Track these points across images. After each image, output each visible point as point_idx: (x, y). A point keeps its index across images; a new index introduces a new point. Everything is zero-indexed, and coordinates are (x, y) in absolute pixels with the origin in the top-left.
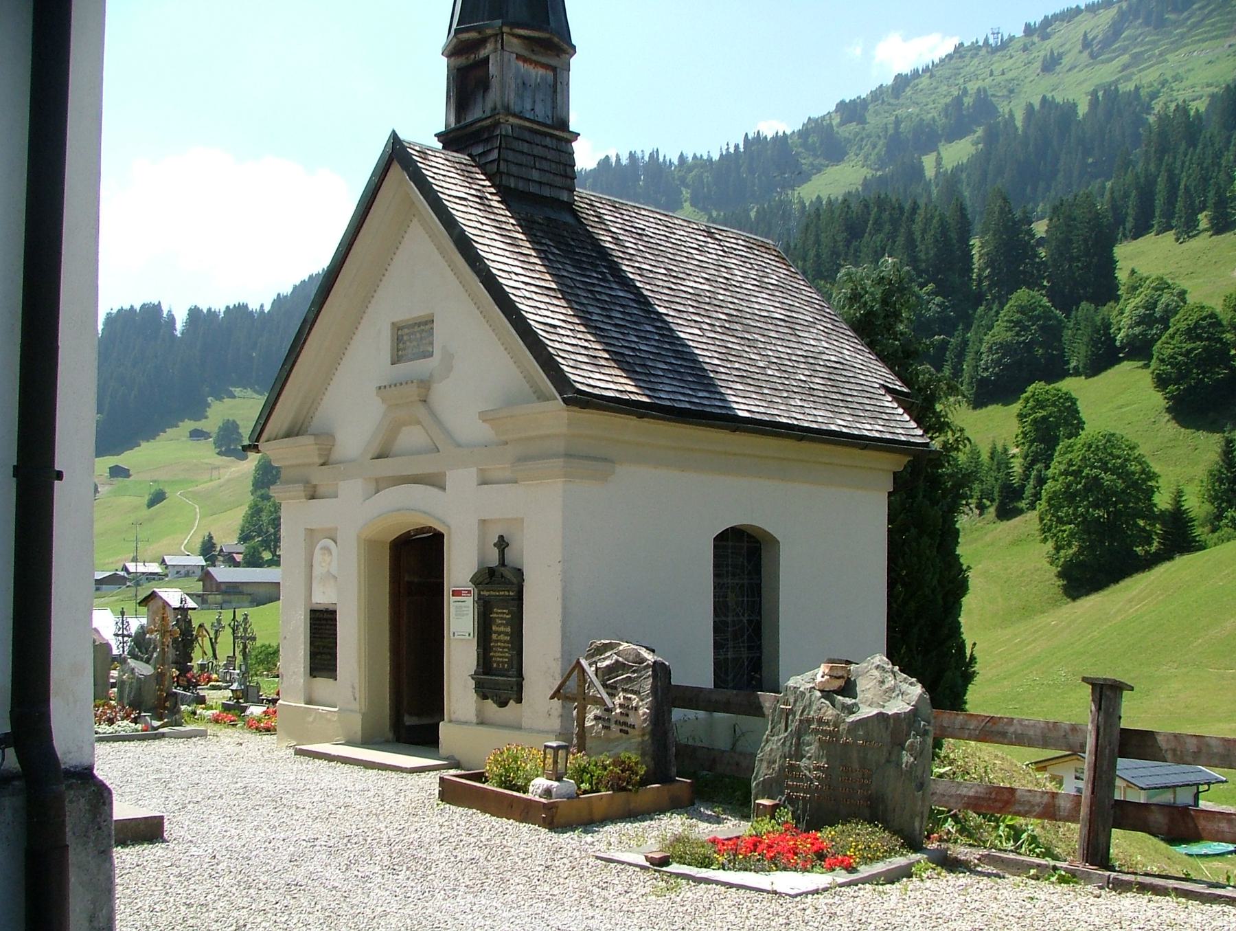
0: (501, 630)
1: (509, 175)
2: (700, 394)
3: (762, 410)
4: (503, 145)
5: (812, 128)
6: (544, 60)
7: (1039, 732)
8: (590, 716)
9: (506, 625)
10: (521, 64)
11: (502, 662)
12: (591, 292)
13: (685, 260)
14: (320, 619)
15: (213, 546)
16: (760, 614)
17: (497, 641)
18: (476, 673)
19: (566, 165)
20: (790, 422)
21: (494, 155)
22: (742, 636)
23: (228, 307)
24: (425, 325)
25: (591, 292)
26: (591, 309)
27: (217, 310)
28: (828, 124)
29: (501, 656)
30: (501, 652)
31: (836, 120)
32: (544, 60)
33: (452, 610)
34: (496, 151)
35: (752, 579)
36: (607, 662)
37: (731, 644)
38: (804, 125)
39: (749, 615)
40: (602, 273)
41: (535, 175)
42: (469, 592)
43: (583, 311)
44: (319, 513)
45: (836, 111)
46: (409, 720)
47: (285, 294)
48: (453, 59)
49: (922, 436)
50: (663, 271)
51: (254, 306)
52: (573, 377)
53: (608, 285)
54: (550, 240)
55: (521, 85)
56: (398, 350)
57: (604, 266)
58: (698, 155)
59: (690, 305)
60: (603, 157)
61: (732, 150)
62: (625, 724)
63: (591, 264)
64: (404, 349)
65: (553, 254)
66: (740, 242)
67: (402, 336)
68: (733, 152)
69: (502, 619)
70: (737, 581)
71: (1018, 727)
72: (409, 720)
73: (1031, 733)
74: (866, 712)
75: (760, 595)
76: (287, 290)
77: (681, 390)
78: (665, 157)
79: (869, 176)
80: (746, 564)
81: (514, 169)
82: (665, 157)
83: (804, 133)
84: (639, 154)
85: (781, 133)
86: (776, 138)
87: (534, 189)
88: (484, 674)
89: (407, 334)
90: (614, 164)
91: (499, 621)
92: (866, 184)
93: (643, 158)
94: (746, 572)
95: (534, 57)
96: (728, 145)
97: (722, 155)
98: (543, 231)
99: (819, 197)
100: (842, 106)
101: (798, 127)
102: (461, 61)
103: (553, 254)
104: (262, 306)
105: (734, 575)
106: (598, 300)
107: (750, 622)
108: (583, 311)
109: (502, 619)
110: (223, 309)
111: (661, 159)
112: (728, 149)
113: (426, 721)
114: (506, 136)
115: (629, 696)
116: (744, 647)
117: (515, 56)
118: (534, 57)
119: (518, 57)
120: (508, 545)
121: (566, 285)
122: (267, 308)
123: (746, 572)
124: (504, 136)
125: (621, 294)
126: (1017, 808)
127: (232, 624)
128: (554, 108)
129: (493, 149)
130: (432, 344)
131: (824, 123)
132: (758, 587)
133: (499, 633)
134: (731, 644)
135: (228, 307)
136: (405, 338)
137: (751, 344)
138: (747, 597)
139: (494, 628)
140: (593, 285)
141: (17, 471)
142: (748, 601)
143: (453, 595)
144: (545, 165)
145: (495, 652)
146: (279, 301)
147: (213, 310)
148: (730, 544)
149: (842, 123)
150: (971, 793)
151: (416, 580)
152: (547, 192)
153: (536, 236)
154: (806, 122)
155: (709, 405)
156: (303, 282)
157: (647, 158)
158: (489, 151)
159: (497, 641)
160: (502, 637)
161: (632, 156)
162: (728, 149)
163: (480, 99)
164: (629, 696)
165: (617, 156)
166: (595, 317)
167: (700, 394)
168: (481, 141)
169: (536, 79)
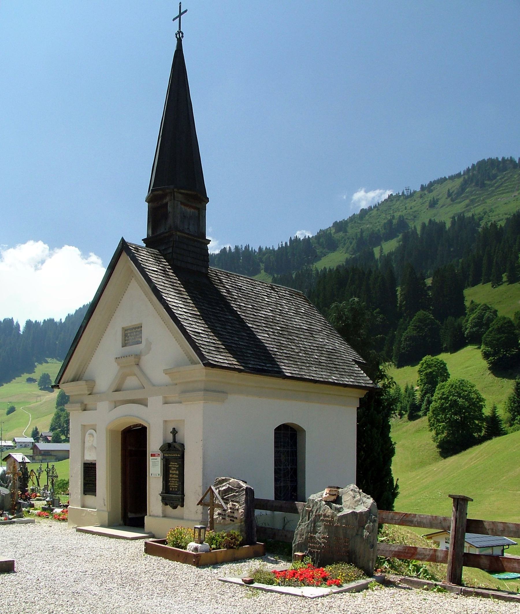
0: (174, 473)
3: (297, 372)
7: (428, 521)
8: (216, 513)
9: (176, 470)
11: (174, 488)
12: (216, 316)
13: (261, 301)
14: (88, 467)
16: (296, 465)
17: (172, 478)
23: (45, 320)
24: (138, 328)
25: (216, 316)
27: (40, 322)
30: (174, 483)
31: (333, 231)
33: (151, 463)
39: (291, 466)
40: (222, 308)
42: (159, 454)
45: (333, 226)
47: (72, 314)
50: (251, 307)
51: (57, 320)
56: (125, 341)
58: (268, 247)
62: (233, 517)
64: (128, 340)
66: (287, 292)
67: (127, 334)
69: (174, 467)
71: (419, 518)
74: (347, 511)
75: (296, 456)
78: (252, 248)
82: (252, 248)
83: (318, 237)
84: (240, 247)
89: (129, 333)
92: (347, 261)
100: (336, 224)
106: (219, 320)
107: (291, 469)
109: (174, 467)
110: (42, 321)
116: (289, 481)
122: (63, 321)
130: (141, 337)
131: (327, 232)
133: (173, 474)
134: (282, 479)
135: (45, 320)
136: (129, 335)
137: (292, 341)
138: (291, 457)
139: (171, 472)
142: (290, 459)
143: (151, 456)
145: (171, 483)
146: (69, 317)
147: (38, 321)
149: (335, 233)
150: (396, 550)
151: (134, 449)
156: (80, 308)
159: (172, 478)
160: (174, 476)
161: (237, 247)
164: (235, 503)
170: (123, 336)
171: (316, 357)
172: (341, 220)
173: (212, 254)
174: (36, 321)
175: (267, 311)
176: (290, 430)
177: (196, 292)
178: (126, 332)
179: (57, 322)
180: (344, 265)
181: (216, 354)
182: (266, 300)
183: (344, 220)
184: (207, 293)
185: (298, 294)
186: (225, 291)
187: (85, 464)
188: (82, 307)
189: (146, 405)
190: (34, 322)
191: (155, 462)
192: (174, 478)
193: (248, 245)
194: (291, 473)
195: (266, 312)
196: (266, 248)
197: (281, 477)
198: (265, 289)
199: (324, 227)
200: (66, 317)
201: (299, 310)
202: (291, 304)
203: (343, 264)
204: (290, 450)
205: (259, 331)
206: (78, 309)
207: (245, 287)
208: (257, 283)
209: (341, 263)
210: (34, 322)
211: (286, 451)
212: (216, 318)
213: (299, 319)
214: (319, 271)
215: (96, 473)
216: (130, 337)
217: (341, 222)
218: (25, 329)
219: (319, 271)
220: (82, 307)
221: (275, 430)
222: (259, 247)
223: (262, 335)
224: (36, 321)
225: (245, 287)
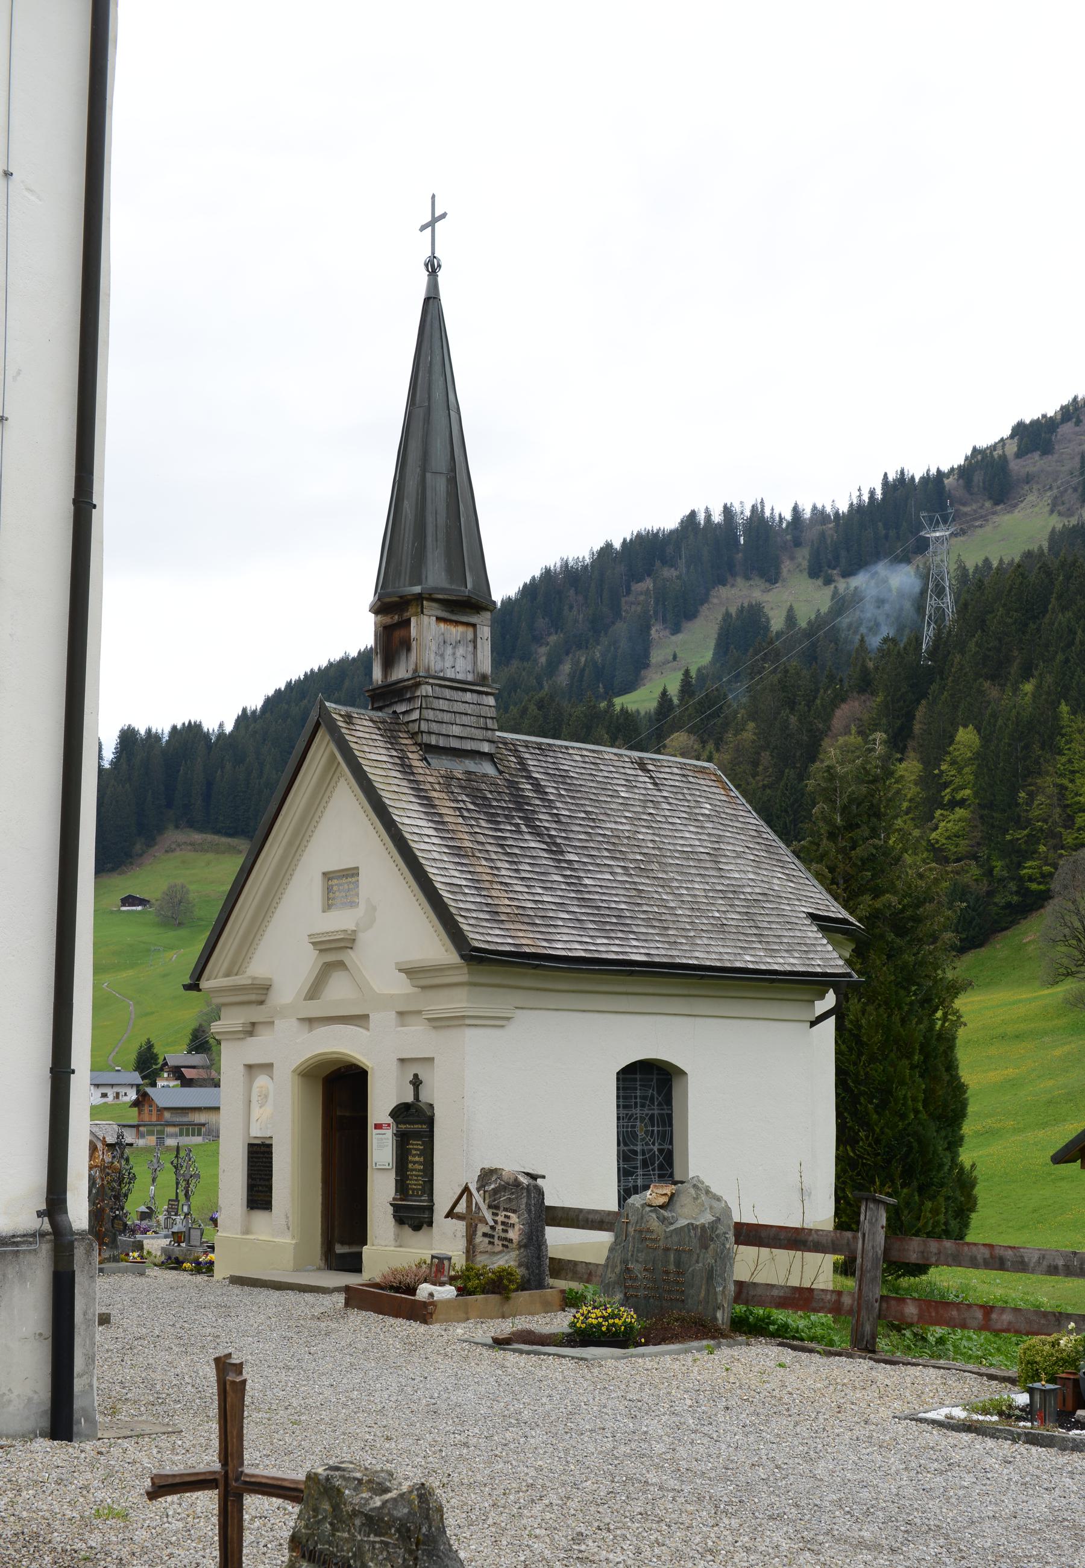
0: (415, 1159)
1: (430, 733)
2: (599, 941)
3: (663, 952)
4: (424, 706)
5: (977, 462)
6: (464, 619)
7: (829, 1239)
8: (479, 1233)
9: (419, 1156)
10: (442, 625)
11: (417, 1189)
12: (502, 846)
13: (609, 799)
14: (257, 1153)
15: (154, 1057)
16: (671, 1143)
17: (412, 1170)
18: (394, 1199)
19: (486, 717)
20: (691, 962)
21: (415, 715)
22: (653, 1164)
23: (174, 728)
24: (352, 873)
25: (502, 846)
26: (499, 864)
27: (160, 731)
28: (1000, 456)
29: (415, 1183)
30: (416, 1180)
31: (1012, 448)
32: (464, 619)
33: (375, 1141)
34: (418, 711)
35: (662, 1109)
36: (492, 1186)
37: (640, 1172)
38: (967, 458)
39: (660, 1144)
40: (517, 825)
41: (456, 730)
42: (389, 1125)
43: (491, 868)
44: (255, 1050)
45: (1012, 436)
46: (340, 1249)
47: (253, 708)
48: (379, 616)
49: (843, 966)
50: (583, 815)
51: (210, 725)
52: (471, 935)
53: (521, 837)
54: (467, 795)
55: (442, 644)
56: (329, 899)
57: (519, 817)
58: (819, 506)
59: (606, 849)
60: (687, 513)
61: (866, 498)
62: (506, 1239)
63: (506, 816)
64: (333, 899)
65: (468, 810)
66: (676, 771)
67: (332, 886)
68: (867, 500)
69: (416, 1150)
70: (647, 1112)
71: (815, 1236)
72: (340, 1249)
73: (824, 1241)
74: (682, 1222)
75: (671, 1125)
76: (255, 703)
77: (579, 939)
78: (772, 509)
79: (1059, 526)
80: (656, 1095)
81: (434, 727)
82: (772, 509)
83: (964, 472)
84: (737, 508)
85: (933, 471)
86: (926, 479)
87: (455, 744)
88: (401, 1200)
89: (336, 885)
90: (702, 522)
91: (414, 1152)
92: (1055, 538)
93: (742, 513)
94: (656, 1103)
95: (454, 618)
96: (859, 490)
97: (851, 505)
98: (461, 787)
99: (987, 561)
100: (1020, 430)
101: (958, 460)
102: (388, 620)
103: (468, 810)
104: (221, 725)
105: (643, 1106)
106: (507, 854)
107: (661, 1151)
108: (491, 868)
109: (416, 1150)
110: (167, 730)
111: (767, 513)
112: (860, 496)
113: (354, 1249)
114: (427, 696)
115: (509, 1214)
116: (654, 1175)
117: (434, 618)
118: (454, 618)
119: (439, 619)
120: (421, 1083)
121: (478, 842)
122: (229, 728)
123: (656, 1103)
124: (425, 696)
125: (533, 845)
126: (814, 1304)
127: (175, 1162)
128: (475, 663)
129: (415, 709)
130: (357, 895)
131: (995, 453)
132: (667, 1120)
133: (415, 1163)
134: (640, 1172)
135: (174, 728)
136: (335, 888)
137: (665, 884)
138: (658, 1127)
139: (410, 1158)
140: (505, 838)
141: (52, 1070)
142: (658, 1131)
143: (375, 1128)
144: (465, 720)
145: (411, 1180)
146: (245, 719)
147: (154, 731)
148: (638, 1076)
149: (1019, 455)
150: (781, 1294)
151: (347, 1114)
152: (469, 745)
153: (452, 793)
154: (969, 453)
155: (606, 952)
156: (278, 692)
157: (748, 513)
158: (412, 710)
159: (412, 1170)
160: (417, 1166)
161: (727, 511)
162: (860, 496)
163: (403, 658)
164: (509, 1214)
165: (707, 510)
166: (504, 872)
167: (599, 941)
168: (404, 700)
169: (456, 636)
170: (323, 891)
171: (717, 915)
172: (1035, 418)
173: (655, 531)
174: (149, 731)
175: (619, 820)
176: (655, 1072)
177: (465, 798)
178: (330, 883)
179: (211, 731)
180: (1043, 550)
181: (491, 928)
182: (623, 794)
183: (1044, 416)
184: (489, 796)
185: (703, 770)
186: (529, 787)
187: (250, 1145)
188: (283, 689)
189: (397, 1012)
190: (142, 732)
191: (382, 1139)
192: (415, 1170)
193: (759, 501)
194: (659, 1159)
195: (616, 822)
196: (815, 508)
197: (637, 1168)
198: (622, 771)
199: (986, 439)
200: (236, 717)
201: (697, 811)
202: (682, 798)
203: (1040, 547)
204: (656, 1112)
205: (592, 868)
206: (271, 693)
207: (578, 770)
208: (606, 757)
209: (1034, 547)
210: (142, 732)
211: (647, 1115)
212: (500, 850)
213: (692, 832)
214: (971, 571)
215: (271, 1163)
216: (337, 893)
217: (1035, 423)
218: (116, 753)
219: (971, 571)
220: (283, 689)
221: (618, 1073)
222: (793, 505)
223: (599, 876)
224: (149, 731)
225: (578, 770)
